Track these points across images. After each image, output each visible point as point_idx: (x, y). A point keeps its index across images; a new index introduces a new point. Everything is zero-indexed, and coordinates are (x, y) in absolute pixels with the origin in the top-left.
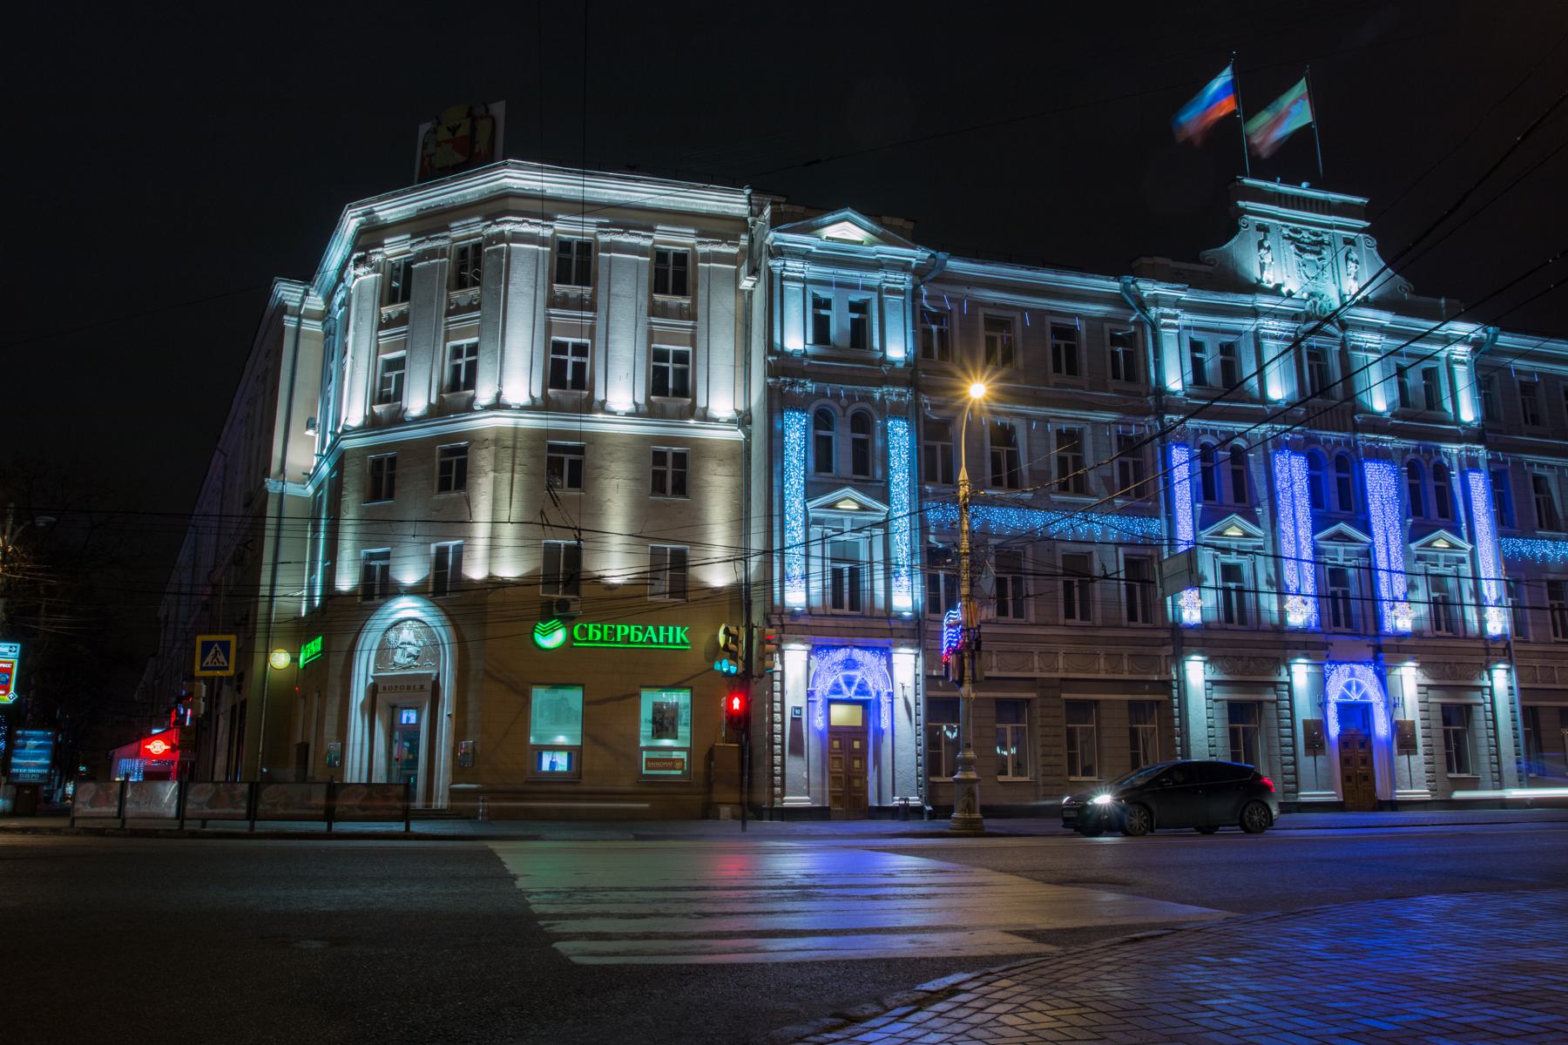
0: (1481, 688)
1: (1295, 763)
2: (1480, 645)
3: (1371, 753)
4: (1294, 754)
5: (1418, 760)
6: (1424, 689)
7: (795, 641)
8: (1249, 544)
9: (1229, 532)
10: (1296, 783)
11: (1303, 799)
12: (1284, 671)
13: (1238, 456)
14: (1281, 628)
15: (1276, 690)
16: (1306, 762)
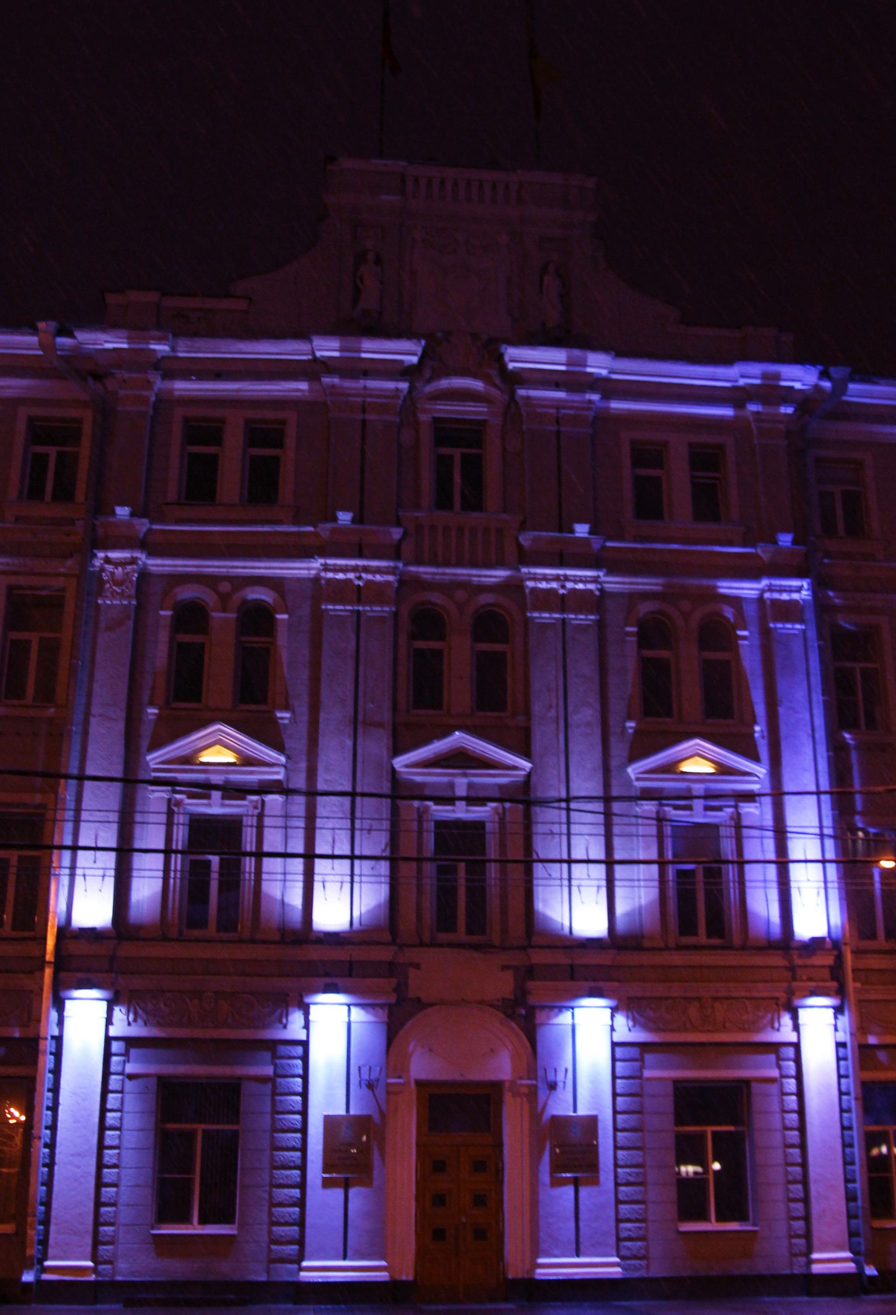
0: (775, 1047)
1: (301, 1203)
2: (778, 960)
3: (499, 1182)
4: (302, 1185)
5: (598, 1198)
6: (634, 1052)
7: (814, 993)
8: (254, 776)
9: (229, 757)
10: (301, 1242)
11: (816, 1268)
12: (297, 1018)
13: (257, 619)
14: (303, 933)
15: (275, 1056)
16: (324, 1203)
